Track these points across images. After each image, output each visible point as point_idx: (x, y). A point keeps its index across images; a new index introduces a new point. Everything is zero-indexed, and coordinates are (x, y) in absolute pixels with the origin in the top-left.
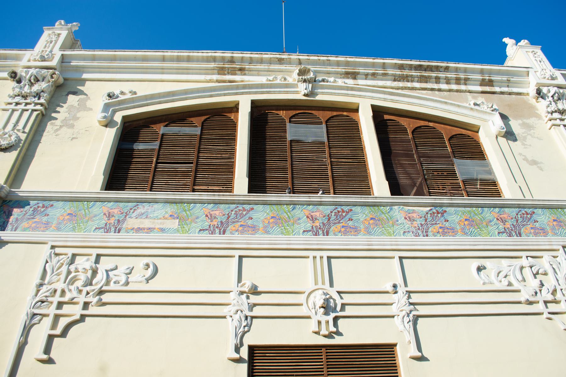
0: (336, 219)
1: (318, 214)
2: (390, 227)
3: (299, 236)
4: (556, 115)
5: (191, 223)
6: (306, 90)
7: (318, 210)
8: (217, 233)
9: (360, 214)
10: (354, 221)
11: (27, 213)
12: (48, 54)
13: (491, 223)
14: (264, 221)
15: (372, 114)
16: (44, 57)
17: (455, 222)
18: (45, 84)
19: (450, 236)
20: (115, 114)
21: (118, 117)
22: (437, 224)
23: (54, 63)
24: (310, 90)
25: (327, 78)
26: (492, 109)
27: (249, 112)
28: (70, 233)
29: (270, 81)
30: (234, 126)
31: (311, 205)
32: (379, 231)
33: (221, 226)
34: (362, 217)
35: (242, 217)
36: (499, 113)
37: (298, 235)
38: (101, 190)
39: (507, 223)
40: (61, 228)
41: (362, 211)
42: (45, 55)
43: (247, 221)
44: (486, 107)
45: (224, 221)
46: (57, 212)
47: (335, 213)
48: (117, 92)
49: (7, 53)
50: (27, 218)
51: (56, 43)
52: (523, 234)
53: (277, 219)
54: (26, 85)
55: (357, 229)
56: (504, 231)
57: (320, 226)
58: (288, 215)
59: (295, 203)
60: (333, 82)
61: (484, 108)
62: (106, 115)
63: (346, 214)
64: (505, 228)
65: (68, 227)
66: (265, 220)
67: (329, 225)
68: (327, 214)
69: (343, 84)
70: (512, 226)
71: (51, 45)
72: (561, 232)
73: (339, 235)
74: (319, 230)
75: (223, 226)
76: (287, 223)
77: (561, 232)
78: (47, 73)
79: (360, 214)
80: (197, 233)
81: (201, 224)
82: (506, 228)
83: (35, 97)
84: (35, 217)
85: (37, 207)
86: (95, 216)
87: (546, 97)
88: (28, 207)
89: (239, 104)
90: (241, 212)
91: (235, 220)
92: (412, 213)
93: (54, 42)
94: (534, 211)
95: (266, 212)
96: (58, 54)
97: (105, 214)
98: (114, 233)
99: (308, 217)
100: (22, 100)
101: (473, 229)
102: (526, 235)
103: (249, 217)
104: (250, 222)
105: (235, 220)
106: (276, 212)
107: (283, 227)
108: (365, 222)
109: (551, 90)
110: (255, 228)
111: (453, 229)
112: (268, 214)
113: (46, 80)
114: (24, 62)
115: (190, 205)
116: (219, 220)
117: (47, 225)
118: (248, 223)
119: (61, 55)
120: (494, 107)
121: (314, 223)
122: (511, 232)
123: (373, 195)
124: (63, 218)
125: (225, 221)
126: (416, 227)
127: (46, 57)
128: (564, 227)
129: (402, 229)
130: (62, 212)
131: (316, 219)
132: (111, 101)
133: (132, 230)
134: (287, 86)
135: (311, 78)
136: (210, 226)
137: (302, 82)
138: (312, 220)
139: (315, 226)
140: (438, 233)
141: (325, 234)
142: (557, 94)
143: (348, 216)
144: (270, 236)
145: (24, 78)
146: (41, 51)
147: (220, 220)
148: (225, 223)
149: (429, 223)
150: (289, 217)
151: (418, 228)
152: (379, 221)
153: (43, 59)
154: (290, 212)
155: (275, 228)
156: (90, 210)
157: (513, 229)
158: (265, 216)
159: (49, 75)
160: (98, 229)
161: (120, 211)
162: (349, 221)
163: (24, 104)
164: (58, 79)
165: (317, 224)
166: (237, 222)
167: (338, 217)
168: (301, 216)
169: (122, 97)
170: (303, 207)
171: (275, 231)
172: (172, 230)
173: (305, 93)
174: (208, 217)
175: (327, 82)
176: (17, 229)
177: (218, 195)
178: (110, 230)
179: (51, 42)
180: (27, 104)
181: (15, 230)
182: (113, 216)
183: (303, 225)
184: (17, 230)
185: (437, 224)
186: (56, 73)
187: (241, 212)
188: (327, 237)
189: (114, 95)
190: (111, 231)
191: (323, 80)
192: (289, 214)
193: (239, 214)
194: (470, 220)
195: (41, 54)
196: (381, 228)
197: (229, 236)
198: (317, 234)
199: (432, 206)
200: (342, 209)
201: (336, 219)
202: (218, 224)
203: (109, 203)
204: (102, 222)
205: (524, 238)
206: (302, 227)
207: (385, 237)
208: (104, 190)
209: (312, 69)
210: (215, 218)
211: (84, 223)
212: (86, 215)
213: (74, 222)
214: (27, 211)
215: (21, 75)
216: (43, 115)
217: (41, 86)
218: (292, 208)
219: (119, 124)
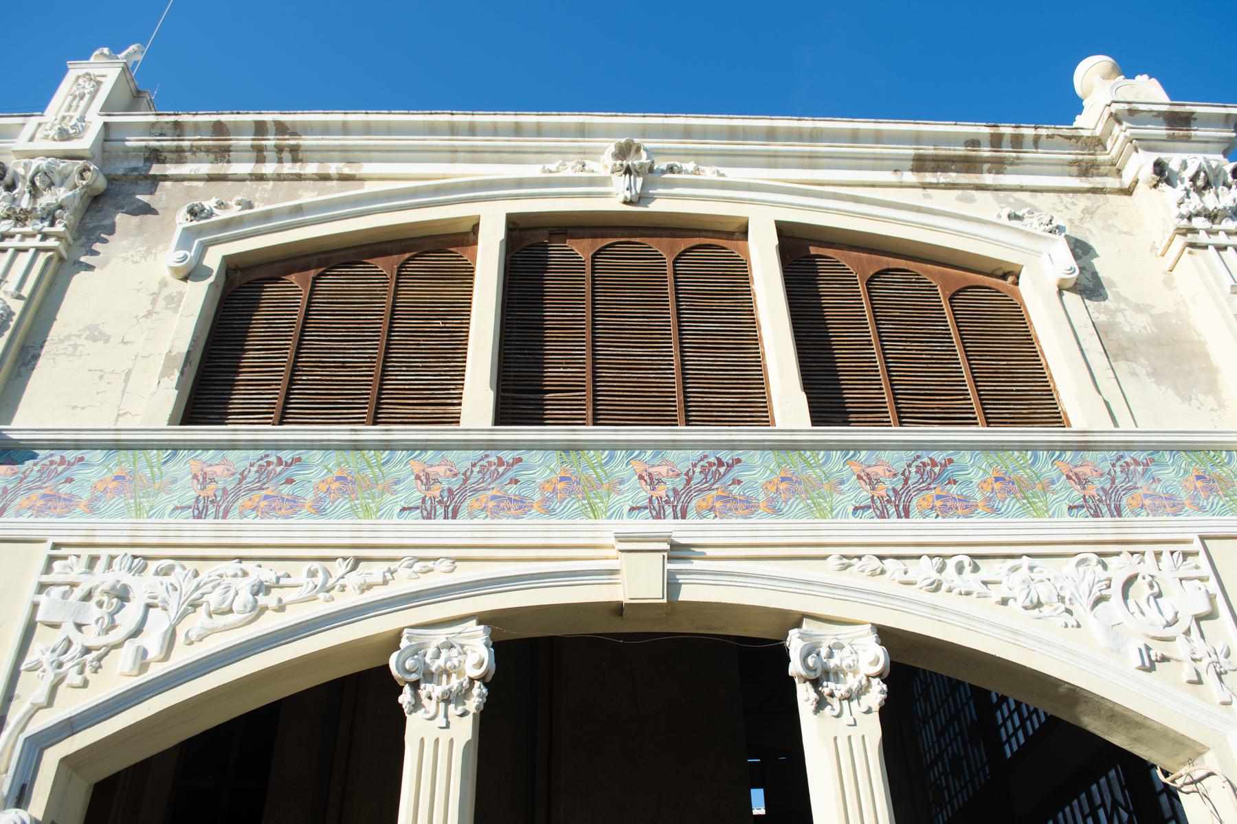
2: (1039, 497)
3: (846, 521)
4: (1199, 222)
5: (381, 495)
6: (629, 192)
7: (445, 462)
11: (25, 477)
12: (75, 125)
13: (1054, 486)
14: (543, 488)
15: (777, 243)
16: (66, 131)
18: (65, 192)
19: (1168, 515)
20: (207, 250)
21: (213, 260)
23: (85, 143)
24: (639, 191)
25: (678, 164)
26: (1050, 226)
27: (501, 242)
30: (466, 275)
32: (800, 506)
34: (976, 476)
35: (719, 479)
36: (1066, 236)
38: (168, 425)
39: (1089, 486)
40: (325, 510)
42: (69, 128)
43: (731, 488)
44: (1036, 224)
47: (1121, 466)
48: (210, 204)
51: (93, 98)
52: (1126, 511)
54: (24, 192)
55: (750, 503)
56: (1083, 503)
57: (667, 496)
59: (176, 445)
61: (1033, 224)
62: (187, 253)
64: (1084, 497)
66: (547, 486)
67: (1116, 492)
68: (463, 471)
69: (715, 177)
70: (1101, 493)
71: (83, 103)
72: (1213, 504)
73: (710, 519)
75: (454, 499)
77: (1213, 504)
78: (70, 168)
80: (850, 514)
82: (1087, 497)
83: (43, 219)
84: (44, 486)
87: (1178, 182)
88: (31, 462)
90: (493, 468)
92: (217, 465)
93: (88, 96)
94: (952, 457)
95: (107, 466)
96: (96, 122)
98: (445, 518)
99: (641, 477)
100: (15, 226)
101: (1011, 500)
102: (1132, 512)
103: (511, 479)
104: (65, 489)
106: (350, 467)
108: (769, 486)
109: (1189, 162)
110: (523, 502)
111: (1172, 499)
113: (69, 182)
114: (21, 143)
115: (1026, 455)
116: (221, 485)
117: (294, 504)
118: (509, 492)
119: (102, 123)
120: (1055, 223)
121: (654, 489)
122: (885, 506)
123: (1069, 425)
124: (328, 486)
125: (1111, 487)
127: (71, 131)
128: (1220, 493)
131: (660, 481)
132: (195, 223)
133: (29, 509)
134: (592, 182)
135: (642, 165)
136: (651, 499)
137: (622, 172)
138: (651, 484)
140: (932, 509)
142: (1202, 174)
144: (1001, 519)
145: (21, 179)
146: (59, 117)
147: (671, 487)
148: (903, 493)
153: (64, 135)
155: (568, 503)
157: (1104, 498)
158: (545, 475)
159: (74, 173)
161: (228, 470)
163: (18, 236)
164: (94, 182)
165: (661, 491)
166: (483, 490)
168: (625, 474)
169: (222, 215)
173: (626, 198)
174: (645, 481)
177: (352, 430)
178: (206, 512)
179: (82, 97)
180: (25, 236)
181: (224, 517)
183: (402, 495)
184: (229, 515)
186: (92, 168)
187: (714, 468)
188: (907, 520)
189: (203, 210)
191: (671, 169)
192: (599, 470)
194: (1004, 479)
195: (59, 126)
196: (579, 501)
197: (918, 520)
198: (884, 513)
199: (705, 448)
200: (931, 459)
202: (441, 496)
203: (205, 452)
204: (189, 494)
205: (1126, 519)
206: (400, 499)
207: (1030, 520)
208: (179, 420)
209: (647, 145)
210: (1086, 482)
211: (374, 498)
212: (154, 480)
213: (352, 496)
214: (28, 472)
215: (15, 173)
216: (61, 259)
217: (56, 195)
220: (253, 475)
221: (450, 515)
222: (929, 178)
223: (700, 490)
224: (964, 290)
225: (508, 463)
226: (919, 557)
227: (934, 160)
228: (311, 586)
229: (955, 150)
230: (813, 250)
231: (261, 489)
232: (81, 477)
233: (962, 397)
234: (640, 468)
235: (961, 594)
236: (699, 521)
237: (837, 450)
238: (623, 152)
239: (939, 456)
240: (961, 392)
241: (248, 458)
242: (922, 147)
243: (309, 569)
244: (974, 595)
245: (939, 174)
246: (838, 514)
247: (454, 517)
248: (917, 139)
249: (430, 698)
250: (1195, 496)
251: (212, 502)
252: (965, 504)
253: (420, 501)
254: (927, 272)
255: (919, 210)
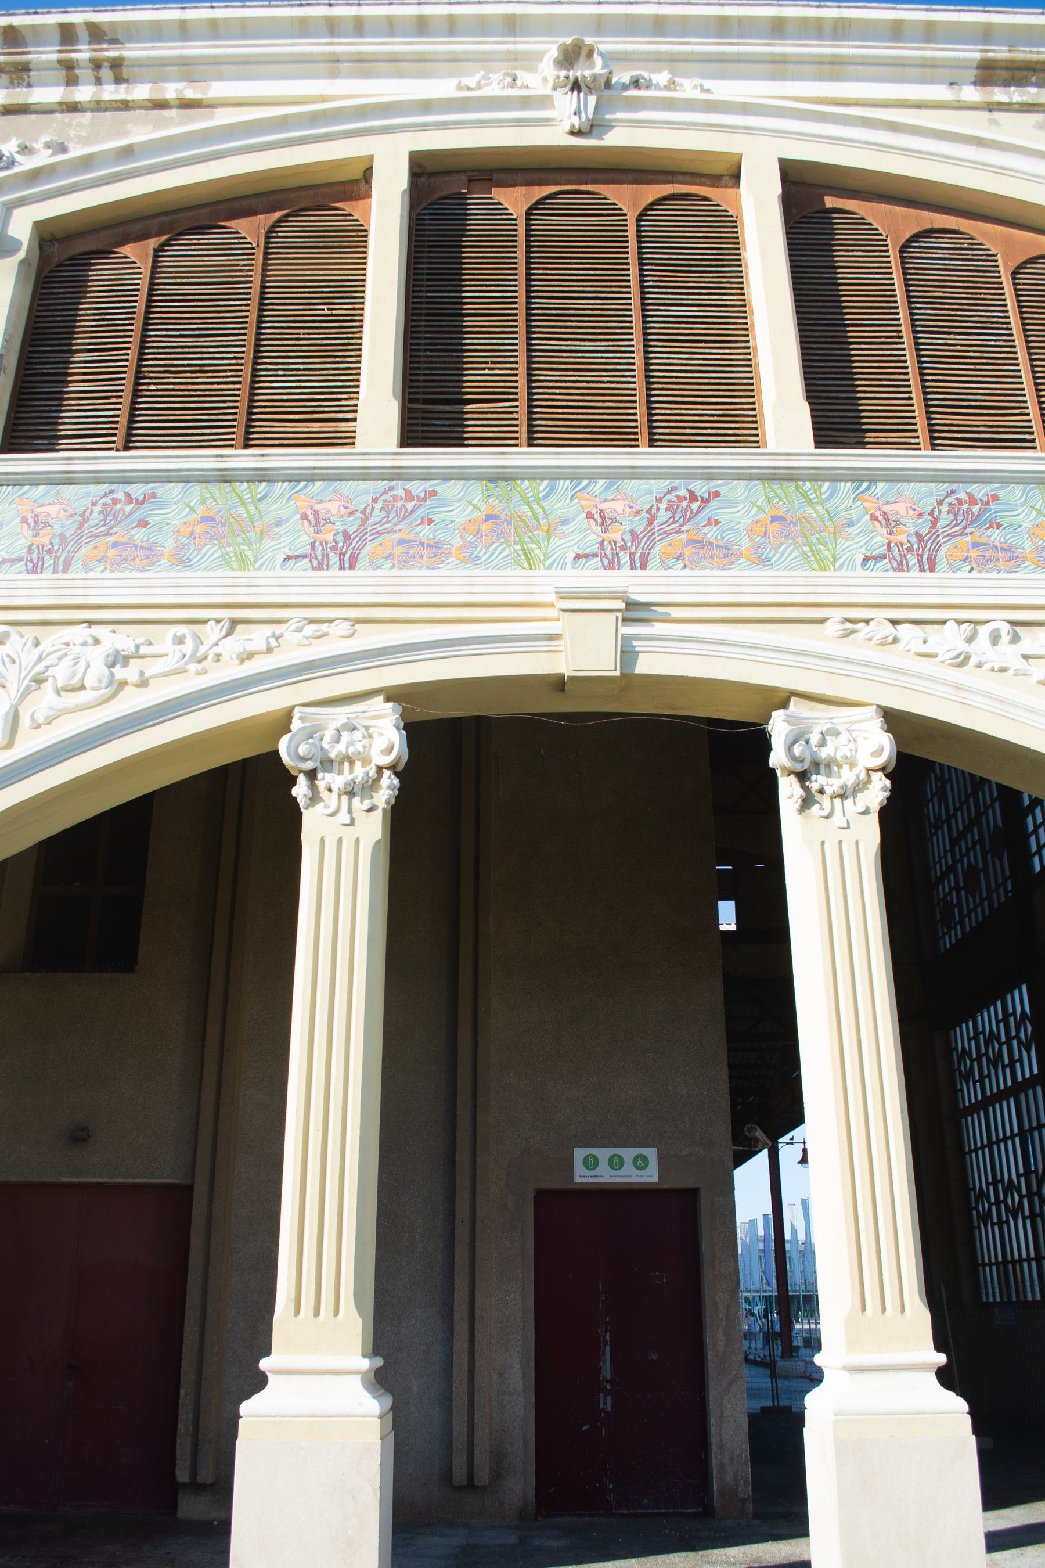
0: (672, 520)
1: (53, 510)
6: (577, 117)
8: (47, 568)
9: (457, 506)
10: (1004, 529)
14: (179, 531)
17: (738, 527)
22: (966, 534)
24: (591, 116)
25: (646, 75)
27: (404, 192)
28: (799, 573)
29: (469, 89)
31: (320, 480)
33: (343, 546)
37: (561, 569)
41: (1025, 500)
43: (706, 530)
45: (639, 529)
46: (739, 511)
49: (36, 22)
50: (90, 534)
53: (790, 524)
55: (729, 549)
56: (598, 551)
57: (909, 542)
58: (248, 511)
60: (665, 86)
63: (700, 506)
65: (786, 554)
68: (361, 508)
69: (697, 95)
73: (677, 570)
74: (909, 556)
76: (530, 534)
79: (1023, 509)
80: (278, 567)
81: (288, 541)
85: (111, 502)
86: (279, 523)
89: (372, 167)
91: (383, 527)
92: (895, 502)
97: (304, 517)
98: (54, 572)
99: (874, 518)
104: (425, 533)
105: (383, 527)
106: (785, 504)
107: (517, 544)
111: (1010, 551)
112: (760, 509)
115: (540, 485)
116: (627, 527)
118: (421, 535)
122: (905, 556)
125: (644, 531)
126: (902, 544)
129: (572, 546)
130: (182, 515)
135: (595, 78)
137: (568, 87)
138: (602, 524)
139: (896, 544)
141: (927, 567)
143: (421, 512)
148: (644, 537)
149: (370, 529)
150: (821, 517)
151: (909, 545)
152: (795, 525)
154: (539, 501)
156: (261, 506)
160: (10, 564)
161: (65, 511)
162: (989, 530)
166: (389, 532)
167: (960, 518)
170: (21, 489)
171: (495, 555)
172: (499, 558)
173: (573, 126)
175: (648, 87)
176: (70, 564)
178: (43, 564)
181: (65, 570)
182: (46, 524)
184: (71, 569)
185: (966, 534)
187: (684, 504)
188: (932, 575)
190: (45, 566)
191: (636, 83)
192: (535, 506)
193: (112, 513)
196: (509, 546)
199: (673, 477)
200: (969, 495)
201: (672, 520)
202: (51, 544)
206: (571, 543)
209: (602, 47)
218: (546, 488)
219: (25, 247)
220: (96, 517)
221: (347, 565)
222: (999, 94)
223: (665, 533)
224: (1033, 260)
225: (418, 498)
226: (944, 622)
227: (1007, 68)
228: (178, 655)
229: (1038, 53)
230: (830, 202)
231: (108, 534)
232: (727, 517)
233: (1017, 411)
234: (303, 505)
235: (993, 670)
236: (663, 573)
237: (846, 481)
238: (570, 56)
239: (980, 491)
240: (1018, 405)
241: (88, 495)
242: (992, 48)
243: (175, 635)
244: (1011, 672)
245: (1012, 89)
246: (842, 565)
247: (352, 567)
248: (986, 34)
249: (330, 790)
250: (762, 544)
251: (622, 548)
252: (435, 550)
253: (885, 547)
254: (985, 234)
255: (980, 142)
